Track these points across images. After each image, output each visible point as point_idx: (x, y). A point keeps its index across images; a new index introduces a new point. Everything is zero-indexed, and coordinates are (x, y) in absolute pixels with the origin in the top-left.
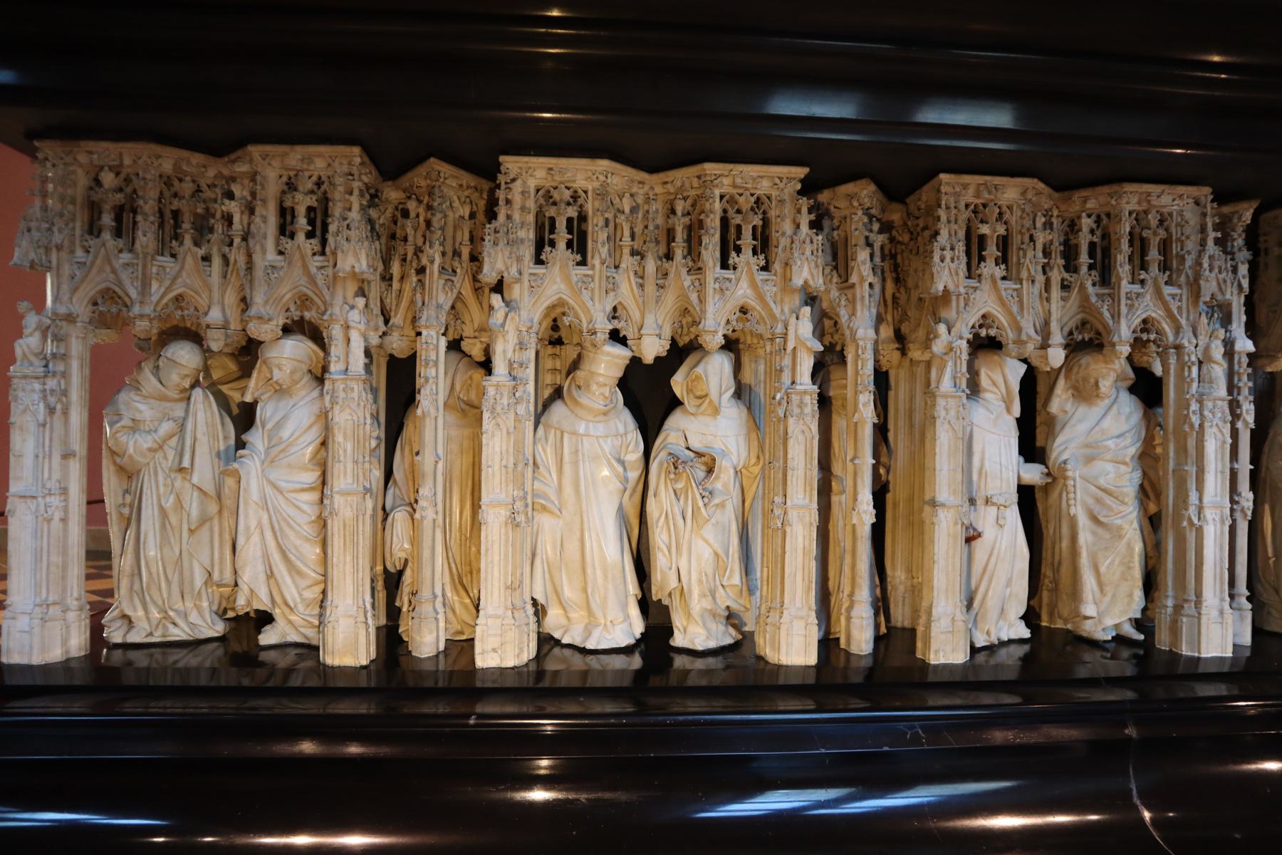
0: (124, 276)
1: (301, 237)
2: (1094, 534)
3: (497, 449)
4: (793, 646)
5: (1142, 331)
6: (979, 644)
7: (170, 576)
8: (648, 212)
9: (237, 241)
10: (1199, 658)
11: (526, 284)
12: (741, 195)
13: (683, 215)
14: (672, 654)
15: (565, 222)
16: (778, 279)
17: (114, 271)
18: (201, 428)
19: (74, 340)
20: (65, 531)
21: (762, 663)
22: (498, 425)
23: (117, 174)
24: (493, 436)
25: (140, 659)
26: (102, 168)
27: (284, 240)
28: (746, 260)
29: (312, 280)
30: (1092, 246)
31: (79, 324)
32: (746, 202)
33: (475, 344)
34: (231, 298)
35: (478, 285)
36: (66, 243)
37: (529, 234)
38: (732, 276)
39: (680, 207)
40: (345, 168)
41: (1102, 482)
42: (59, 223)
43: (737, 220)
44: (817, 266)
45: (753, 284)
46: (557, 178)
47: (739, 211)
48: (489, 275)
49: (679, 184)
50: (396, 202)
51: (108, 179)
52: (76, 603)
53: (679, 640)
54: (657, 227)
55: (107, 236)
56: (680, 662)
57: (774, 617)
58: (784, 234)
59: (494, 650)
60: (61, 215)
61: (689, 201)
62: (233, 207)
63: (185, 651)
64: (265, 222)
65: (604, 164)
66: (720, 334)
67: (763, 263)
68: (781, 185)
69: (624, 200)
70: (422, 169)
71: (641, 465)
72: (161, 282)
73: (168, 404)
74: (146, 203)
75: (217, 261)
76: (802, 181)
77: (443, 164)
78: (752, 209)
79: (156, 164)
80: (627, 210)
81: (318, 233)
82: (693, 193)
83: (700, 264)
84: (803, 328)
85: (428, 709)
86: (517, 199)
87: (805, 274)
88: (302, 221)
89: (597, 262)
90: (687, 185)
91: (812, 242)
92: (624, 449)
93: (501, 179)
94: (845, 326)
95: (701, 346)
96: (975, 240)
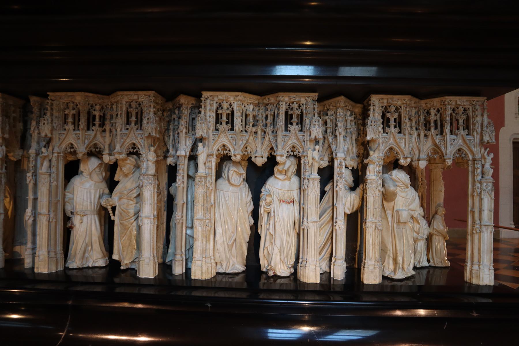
4: (311, 275)
28: (294, 128)
30: (436, 121)
51: (134, 105)
81: (139, 122)
85: (180, 293)
89: (475, 133)
93: (202, 99)
96: (386, 119)
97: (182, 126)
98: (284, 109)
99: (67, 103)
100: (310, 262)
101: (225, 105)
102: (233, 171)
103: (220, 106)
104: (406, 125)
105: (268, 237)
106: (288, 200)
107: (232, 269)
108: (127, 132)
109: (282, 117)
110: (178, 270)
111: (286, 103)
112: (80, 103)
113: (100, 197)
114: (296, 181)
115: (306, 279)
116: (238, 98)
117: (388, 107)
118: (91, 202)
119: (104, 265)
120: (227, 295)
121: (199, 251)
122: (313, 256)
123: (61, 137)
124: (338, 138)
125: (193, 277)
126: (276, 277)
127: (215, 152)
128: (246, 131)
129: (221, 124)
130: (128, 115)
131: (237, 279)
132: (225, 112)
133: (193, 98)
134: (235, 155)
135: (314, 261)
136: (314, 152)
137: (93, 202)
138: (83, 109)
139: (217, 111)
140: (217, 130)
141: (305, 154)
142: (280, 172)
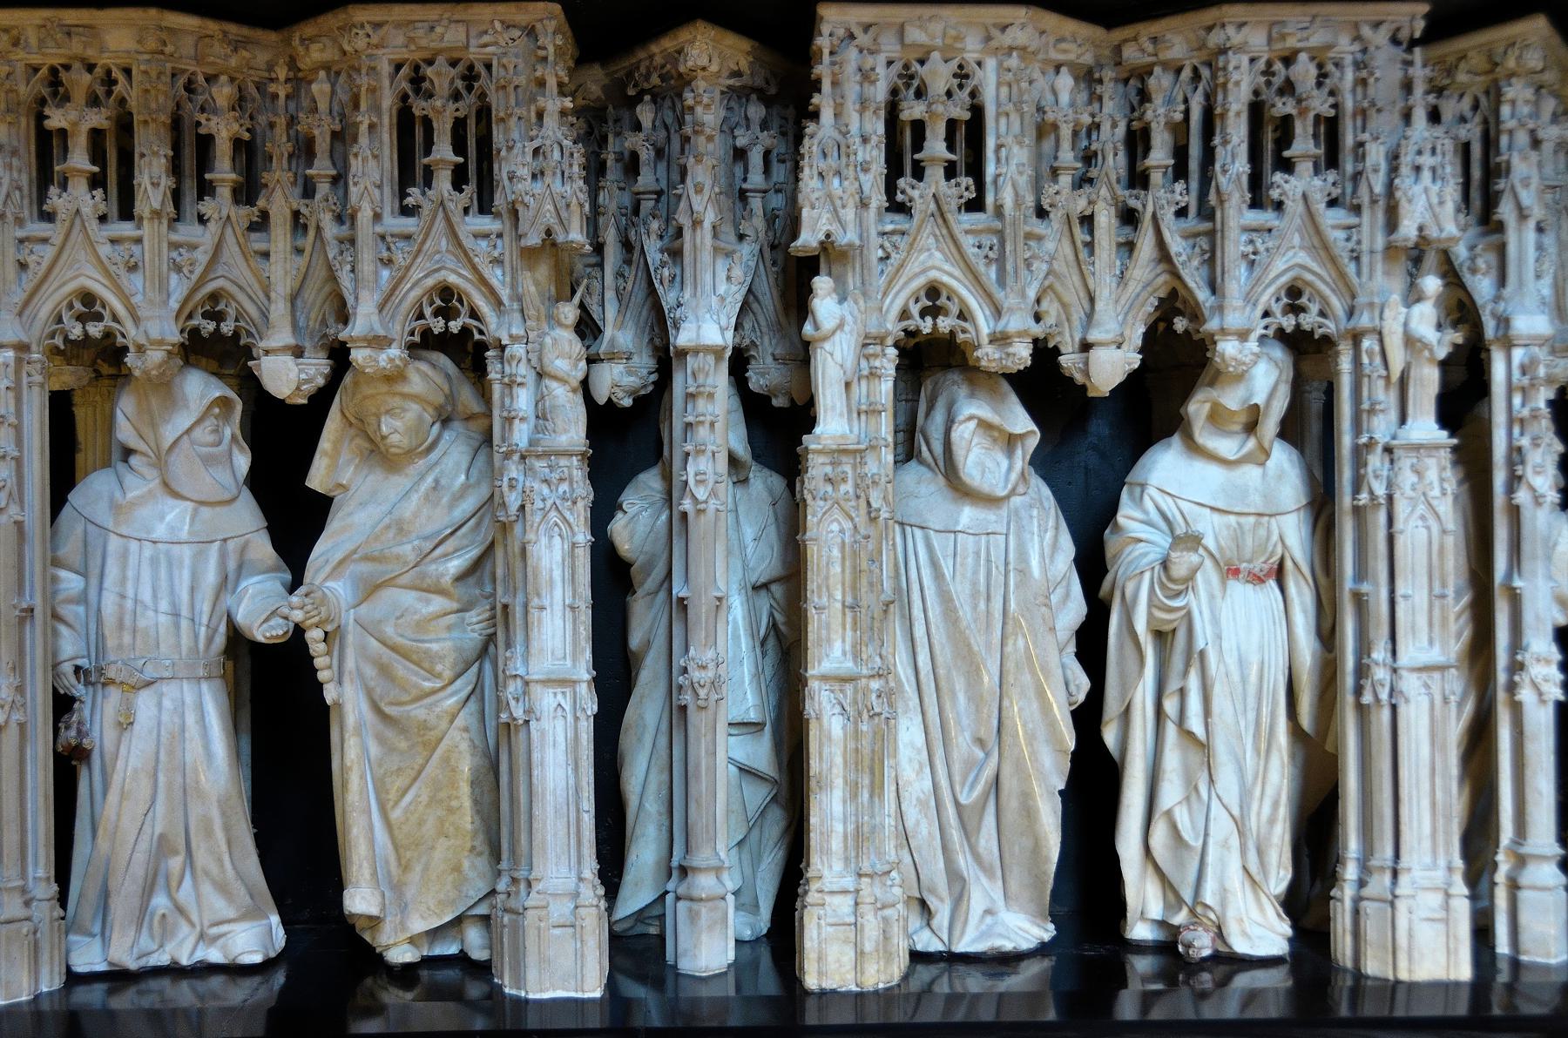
1: (935, 174)
2: (381, 740)
5: (924, 313)
6: (81, 966)
10: (527, 1001)
15: (449, 126)
37: (875, 155)
41: (389, 631)
43: (1283, 107)
51: (441, 77)
97: (699, 189)
98: (388, 101)
99: (54, 71)
100: (1417, 873)
101: (939, 76)
102: (972, 424)
103: (909, 82)
104: (1009, 163)
105: (1172, 759)
106: (1258, 565)
107: (983, 936)
108: (409, 225)
109: (1237, 131)
110: (709, 948)
111: (1252, 60)
112: (127, 72)
113: (225, 583)
114: (1287, 466)
115: (1403, 963)
116: (1007, 39)
117: (916, 67)
118: (176, 615)
119: (257, 958)
121: (836, 844)
122: (1427, 844)
123: (31, 259)
124: (1512, 237)
125: (811, 982)
126: (1229, 962)
127: (893, 328)
128: (1041, 213)
129: (428, 183)
130: (411, 134)
131: (1017, 982)
132: (937, 112)
133: (745, 44)
134: (141, 349)
135: (1434, 866)
136: (1417, 309)
137: (185, 612)
138: (148, 101)
140: (898, 207)
141: (1364, 320)
142: (1217, 417)
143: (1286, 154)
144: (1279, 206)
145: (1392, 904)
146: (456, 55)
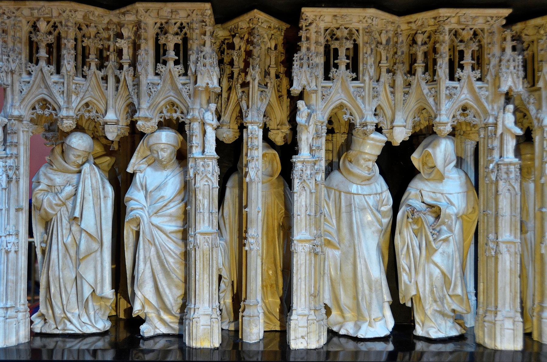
0: (55, 90)
1: (171, 64)
3: (303, 203)
7: (69, 290)
8: (397, 42)
9: (126, 67)
11: (320, 94)
12: (463, 29)
13: (422, 45)
14: (415, 341)
16: (490, 86)
17: (47, 87)
18: (89, 190)
19: (21, 133)
20: (17, 258)
21: (481, 350)
22: (304, 187)
23: (48, 22)
24: (300, 195)
25: (51, 343)
26: (38, 19)
27: (159, 66)
29: (179, 93)
31: (24, 122)
32: (467, 35)
33: (278, 134)
34: (121, 104)
35: (280, 94)
36: (17, 69)
37: (320, 60)
38: (458, 85)
39: (420, 39)
40: (200, 18)
42: (13, 56)
44: (518, 77)
45: (472, 91)
46: (340, 22)
47: (461, 41)
48: (296, 88)
49: (420, 23)
50: (222, 38)
51: (43, 26)
52: (22, 307)
53: (419, 331)
54: (403, 53)
55: (43, 63)
56: (420, 346)
57: (490, 317)
58: (494, 55)
59: (303, 337)
60: (14, 51)
61: (426, 35)
62: (123, 44)
63: (77, 341)
64: (147, 54)
65: (372, 11)
66: (449, 125)
67: (479, 76)
68: (492, 22)
69: (382, 35)
70: (246, 17)
71: (391, 214)
72: (77, 95)
73: (70, 175)
74: (69, 42)
75: (111, 81)
76: (506, 18)
77: (262, 13)
78: (471, 39)
79: (74, 16)
80: (384, 42)
81: (181, 61)
82: (429, 29)
83: (436, 78)
84: (509, 119)
86: (313, 36)
87: (510, 83)
88: (171, 54)
89: (367, 78)
90: (426, 24)
91: (514, 61)
92: (380, 203)
93: (303, 23)
94: (534, 117)
95: (434, 133)
120: (2, 275)
132: (44, 39)
139: (157, 40)
143: (462, 62)
144: (459, 80)
145: (495, 324)
146: (49, 20)
